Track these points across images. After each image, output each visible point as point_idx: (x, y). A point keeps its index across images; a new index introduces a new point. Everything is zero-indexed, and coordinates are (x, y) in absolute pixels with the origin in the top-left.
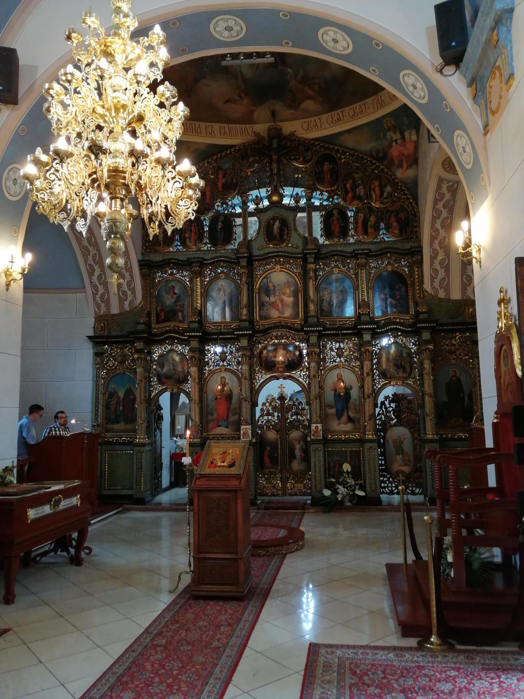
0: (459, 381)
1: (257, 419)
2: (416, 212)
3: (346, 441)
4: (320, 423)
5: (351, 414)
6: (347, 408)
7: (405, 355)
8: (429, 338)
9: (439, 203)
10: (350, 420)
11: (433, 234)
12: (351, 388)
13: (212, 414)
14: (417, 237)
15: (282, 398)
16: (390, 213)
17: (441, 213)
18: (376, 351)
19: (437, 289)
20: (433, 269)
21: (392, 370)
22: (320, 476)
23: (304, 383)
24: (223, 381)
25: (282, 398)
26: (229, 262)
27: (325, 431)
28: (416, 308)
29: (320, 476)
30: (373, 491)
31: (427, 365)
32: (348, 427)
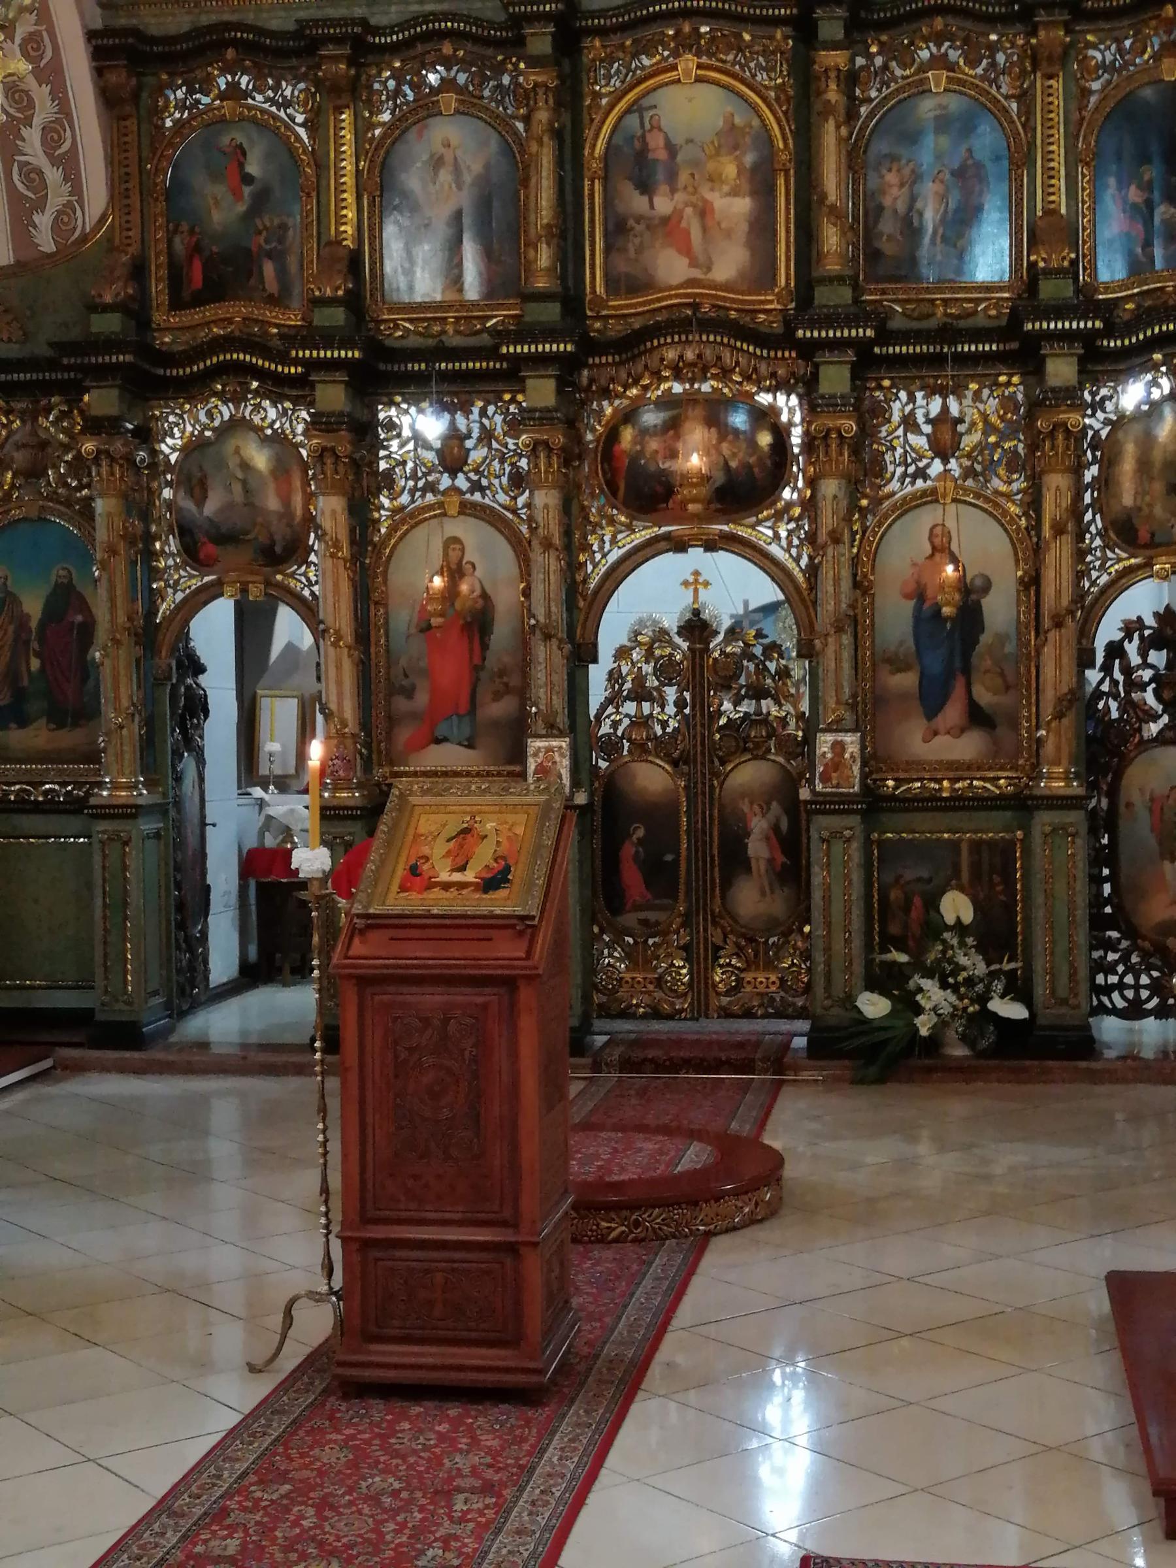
1: (593, 712)
3: (958, 803)
5: (984, 696)
6: (967, 671)
10: (978, 717)
12: (987, 587)
13: (409, 693)
18: (1097, 433)
22: (847, 942)
23: (791, 565)
26: (475, 39)
27: (871, 761)
29: (847, 942)
30: (1064, 1002)
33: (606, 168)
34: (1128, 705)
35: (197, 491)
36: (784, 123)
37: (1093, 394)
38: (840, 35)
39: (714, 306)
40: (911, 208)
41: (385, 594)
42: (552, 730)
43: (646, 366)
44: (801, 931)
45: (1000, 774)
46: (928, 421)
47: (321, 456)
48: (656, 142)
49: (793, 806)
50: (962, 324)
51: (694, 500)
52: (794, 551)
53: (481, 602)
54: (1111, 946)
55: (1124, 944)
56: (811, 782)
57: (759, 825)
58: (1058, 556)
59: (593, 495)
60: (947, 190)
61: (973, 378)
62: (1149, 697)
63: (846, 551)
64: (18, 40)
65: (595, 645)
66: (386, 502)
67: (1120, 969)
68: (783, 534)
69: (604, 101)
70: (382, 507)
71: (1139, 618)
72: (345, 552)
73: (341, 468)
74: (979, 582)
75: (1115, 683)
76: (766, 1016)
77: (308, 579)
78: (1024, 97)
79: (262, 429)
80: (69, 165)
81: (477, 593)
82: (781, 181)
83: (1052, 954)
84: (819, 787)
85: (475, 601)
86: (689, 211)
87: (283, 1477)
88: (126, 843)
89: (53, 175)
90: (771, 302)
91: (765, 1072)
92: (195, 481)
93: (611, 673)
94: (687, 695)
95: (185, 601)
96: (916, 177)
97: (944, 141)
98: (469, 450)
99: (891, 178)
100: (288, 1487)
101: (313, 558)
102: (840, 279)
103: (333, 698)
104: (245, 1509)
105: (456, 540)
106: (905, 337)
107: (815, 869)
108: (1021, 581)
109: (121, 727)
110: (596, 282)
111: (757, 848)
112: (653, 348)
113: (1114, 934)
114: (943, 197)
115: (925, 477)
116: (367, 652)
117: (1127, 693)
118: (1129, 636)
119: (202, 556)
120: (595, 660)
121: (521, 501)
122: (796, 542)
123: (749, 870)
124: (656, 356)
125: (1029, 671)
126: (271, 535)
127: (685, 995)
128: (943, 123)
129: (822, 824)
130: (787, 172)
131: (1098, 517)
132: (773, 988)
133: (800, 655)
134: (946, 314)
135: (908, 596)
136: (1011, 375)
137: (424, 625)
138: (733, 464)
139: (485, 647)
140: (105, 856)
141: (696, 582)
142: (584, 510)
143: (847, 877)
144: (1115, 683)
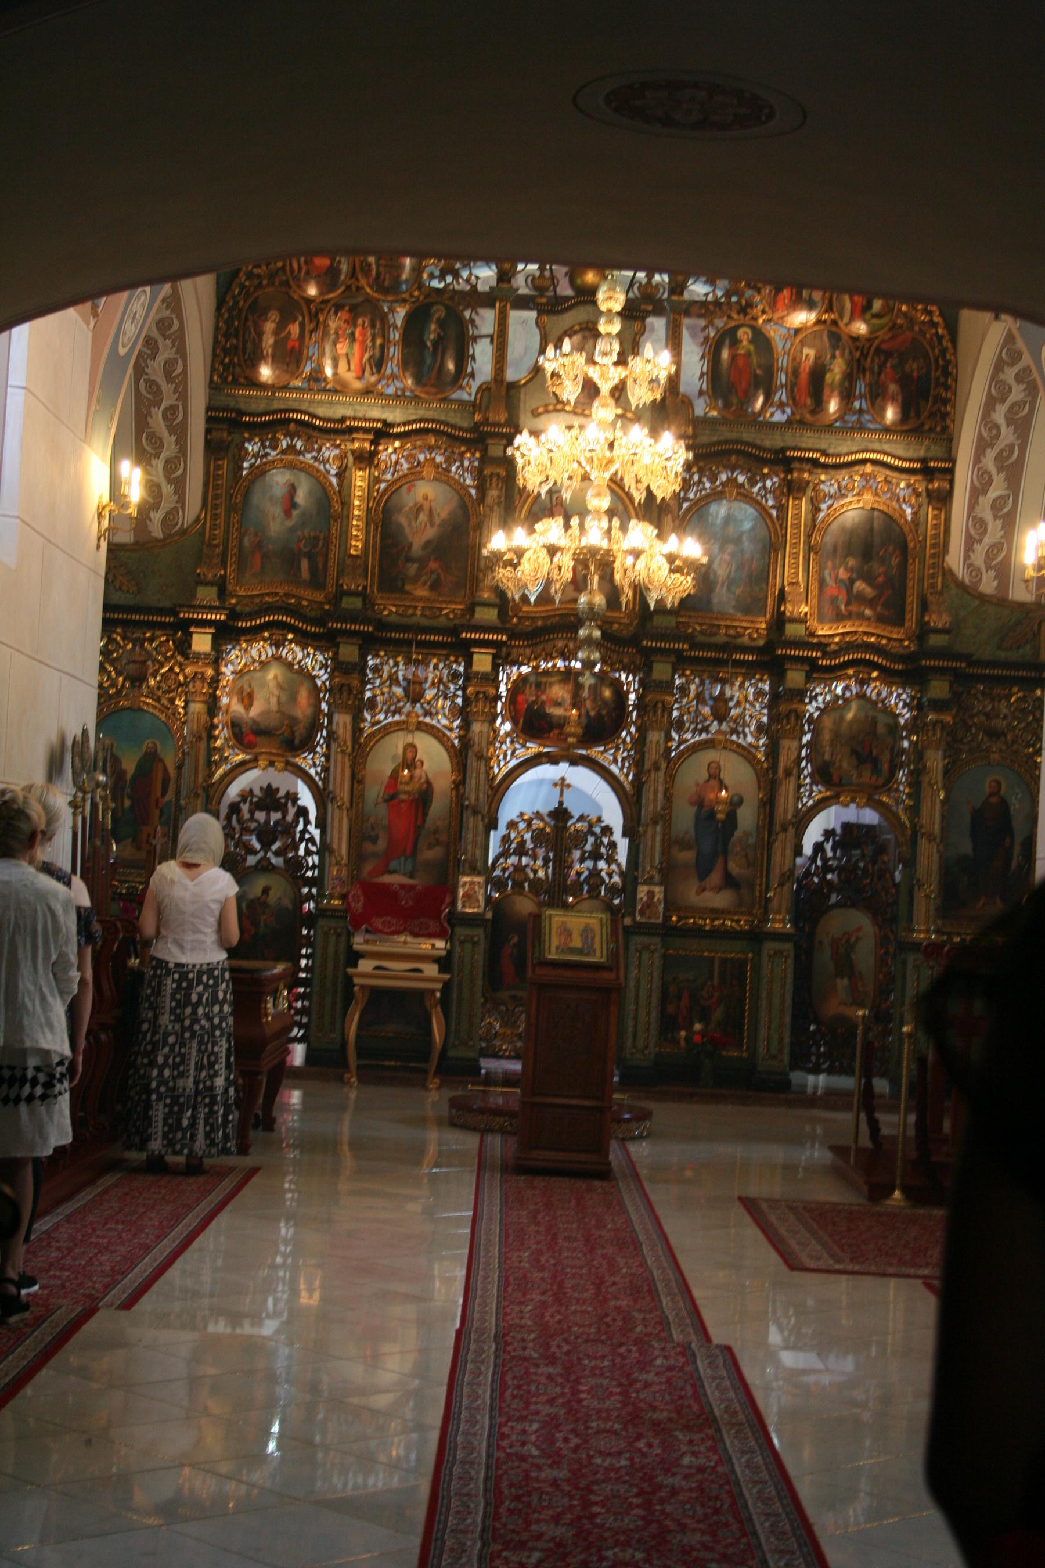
0: (1004, 807)
1: (490, 861)
2: (948, 362)
3: (717, 934)
4: (660, 884)
5: (734, 868)
6: (725, 853)
7: (881, 729)
8: (948, 696)
9: (1006, 369)
10: (730, 882)
11: (985, 434)
12: (740, 802)
13: (374, 840)
14: (945, 429)
15: (560, 814)
16: (882, 358)
17: (1010, 390)
18: (811, 715)
19: (979, 569)
20: (974, 518)
21: (845, 764)
22: (648, 1014)
23: (622, 778)
24: (410, 755)
25: (560, 814)
26: (449, 436)
27: (670, 904)
28: (923, 616)
29: (648, 1014)
30: (774, 1057)
31: (935, 761)
32: (721, 900)
35: (246, 700)
41: (363, 777)
43: (544, 649)
52: (625, 770)
61: (434, 655)
64: (162, 408)
68: (620, 760)
72: (349, 750)
78: (782, 508)
81: (423, 779)
92: (245, 694)
94: (551, 855)
98: (730, 709)
103: (336, 840)
108: (454, 782)
112: (549, 640)
115: (708, 732)
118: (827, 840)
119: (246, 741)
125: (762, 854)
126: (293, 733)
129: (638, 940)
131: (809, 766)
134: (726, 634)
135: (692, 804)
139: (425, 814)
143: (651, 974)
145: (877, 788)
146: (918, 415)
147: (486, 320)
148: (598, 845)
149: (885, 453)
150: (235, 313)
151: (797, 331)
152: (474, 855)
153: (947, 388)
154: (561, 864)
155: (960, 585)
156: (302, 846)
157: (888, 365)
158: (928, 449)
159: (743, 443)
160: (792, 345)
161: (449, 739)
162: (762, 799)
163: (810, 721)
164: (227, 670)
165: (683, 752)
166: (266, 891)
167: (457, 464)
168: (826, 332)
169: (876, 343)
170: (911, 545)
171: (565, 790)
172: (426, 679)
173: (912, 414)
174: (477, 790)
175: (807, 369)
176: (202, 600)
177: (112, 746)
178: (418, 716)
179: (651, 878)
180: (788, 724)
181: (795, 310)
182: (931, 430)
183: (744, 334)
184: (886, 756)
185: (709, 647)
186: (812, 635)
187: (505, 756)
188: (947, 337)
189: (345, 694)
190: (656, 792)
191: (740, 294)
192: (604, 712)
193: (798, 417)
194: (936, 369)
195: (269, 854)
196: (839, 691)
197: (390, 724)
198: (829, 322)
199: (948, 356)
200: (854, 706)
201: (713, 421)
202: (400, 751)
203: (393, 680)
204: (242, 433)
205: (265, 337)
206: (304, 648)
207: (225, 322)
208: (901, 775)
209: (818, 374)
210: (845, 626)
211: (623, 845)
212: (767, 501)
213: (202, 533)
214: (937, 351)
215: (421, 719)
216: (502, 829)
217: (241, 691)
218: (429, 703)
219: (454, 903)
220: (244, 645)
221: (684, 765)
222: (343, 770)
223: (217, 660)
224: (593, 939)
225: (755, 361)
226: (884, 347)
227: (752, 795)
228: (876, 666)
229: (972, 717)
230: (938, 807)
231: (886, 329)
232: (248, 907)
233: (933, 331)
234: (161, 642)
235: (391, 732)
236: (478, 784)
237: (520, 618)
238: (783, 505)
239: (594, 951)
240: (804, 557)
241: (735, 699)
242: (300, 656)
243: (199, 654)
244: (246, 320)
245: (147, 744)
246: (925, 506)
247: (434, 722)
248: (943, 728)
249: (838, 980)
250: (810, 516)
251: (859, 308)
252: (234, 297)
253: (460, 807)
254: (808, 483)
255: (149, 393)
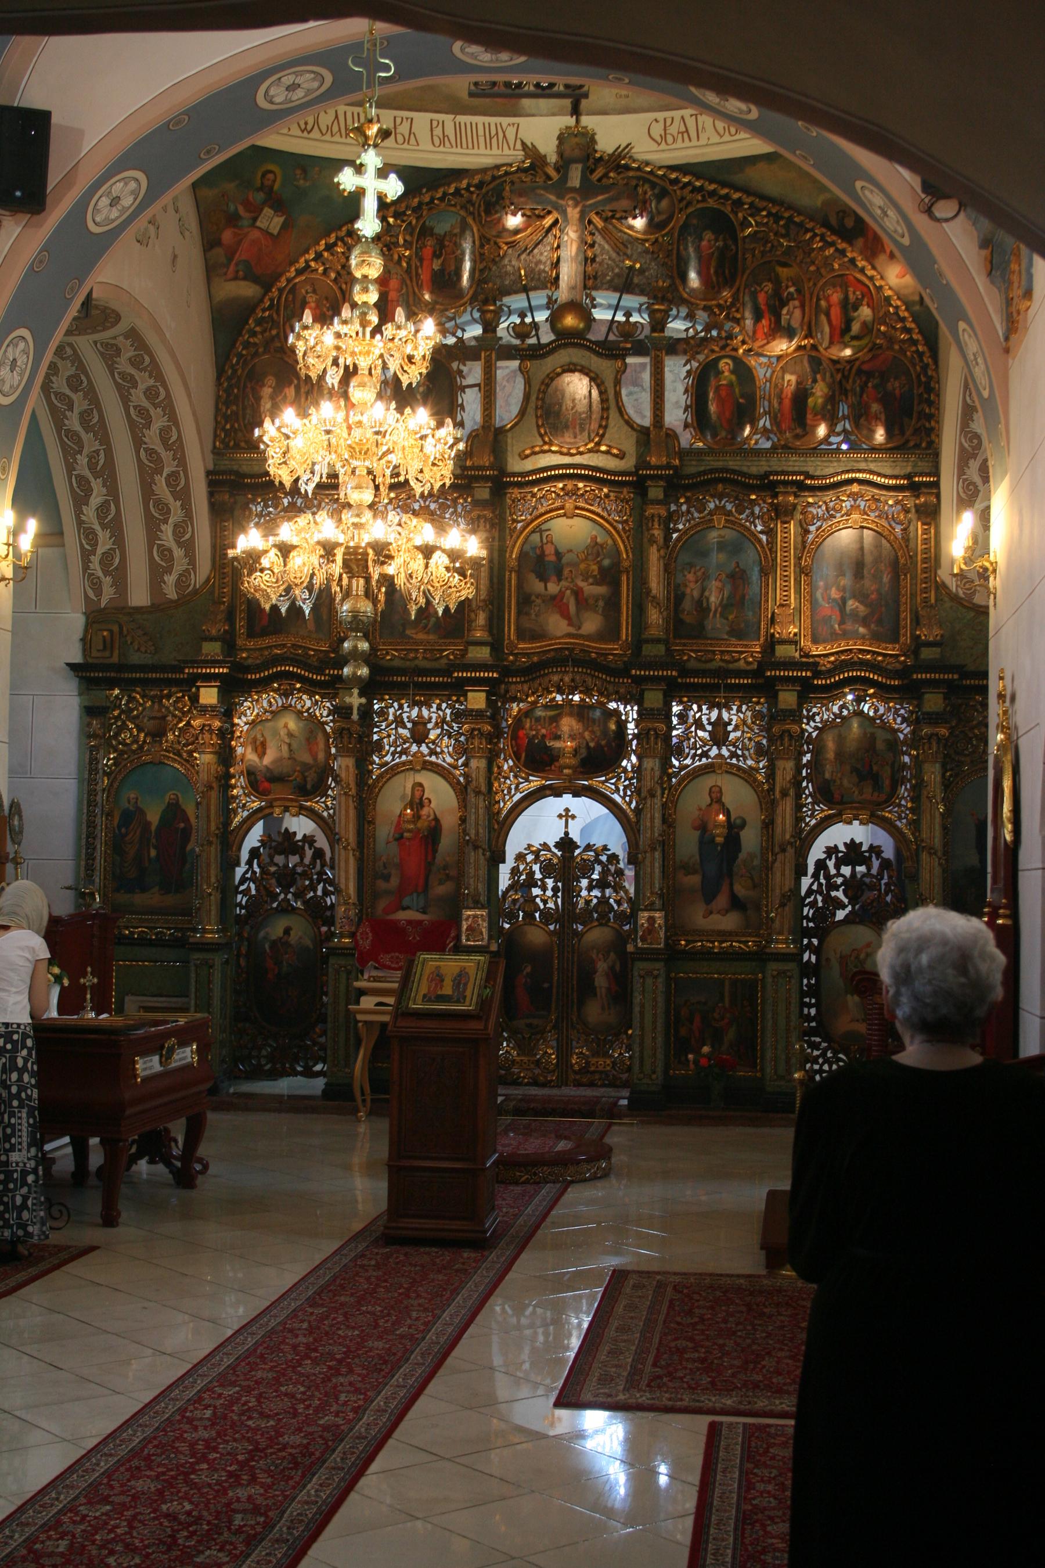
3: (726, 956)
5: (740, 890)
6: (730, 874)
7: (880, 745)
10: (736, 904)
11: (966, 445)
12: (743, 824)
13: (387, 878)
14: (931, 443)
15: (566, 844)
16: (864, 379)
22: (654, 1039)
24: (418, 794)
27: (674, 928)
29: (654, 1039)
32: (729, 922)
33: (519, 566)
34: (827, 899)
35: (260, 749)
36: (627, 543)
37: (808, 711)
38: (661, 496)
39: (581, 650)
40: (702, 595)
42: (477, 905)
44: (626, 1033)
45: (749, 939)
46: (710, 723)
47: (341, 733)
48: (549, 550)
49: (623, 955)
50: (731, 666)
51: (568, 767)
52: (627, 799)
53: (433, 823)
54: (815, 1046)
55: (824, 1045)
56: (635, 940)
57: (602, 966)
58: (787, 807)
59: (505, 760)
60: (724, 586)
61: (437, 696)
62: (839, 894)
63: (658, 802)
64: (164, 475)
65: (504, 852)
66: (377, 760)
67: (821, 1060)
68: (621, 788)
69: (519, 525)
70: (374, 762)
71: (836, 846)
72: (353, 792)
73: (353, 740)
74: (738, 822)
75: (820, 885)
76: (603, 1086)
77: (327, 806)
78: (770, 532)
79: (302, 713)
80: (189, 547)
81: (432, 817)
82: (624, 578)
83: (776, 1049)
84: (640, 944)
85: (430, 821)
86: (568, 592)
87: (106, 1500)
88: (211, 967)
89: (178, 553)
90: (616, 649)
91: (602, 1118)
92: (258, 743)
93: (513, 869)
94: (560, 884)
95: (248, 817)
96: (706, 577)
97: (722, 557)
99: (691, 577)
100: (108, 1507)
101: (330, 792)
102: (658, 641)
103: (343, 881)
104: (74, 1522)
105: (421, 785)
106: (696, 673)
107: (636, 994)
109: (210, 894)
110: (511, 631)
111: (601, 981)
113: (818, 1039)
114: (721, 590)
115: (708, 757)
116: (362, 853)
117: (828, 891)
119: (261, 789)
120: (504, 862)
121: (460, 762)
122: (629, 793)
123: (595, 995)
124: (546, 679)
127: (554, 1071)
128: (722, 546)
129: (641, 966)
130: (628, 572)
132: (608, 1068)
133: (630, 862)
134: (721, 660)
135: (696, 829)
136: (760, 698)
137: (397, 836)
138: (592, 745)
139: (435, 851)
140: (197, 975)
141: (567, 815)
142: (500, 768)
143: (655, 999)
144: (820, 885)
145: (879, 804)
146: (902, 433)
147: (473, 372)
148: (604, 873)
149: (871, 472)
150: (233, 381)
151: (779, 358)
152: (476, 889)
153: (930, 403)
154: (569, 892)
155: (955, 598)
156: (320, 887)
157: (870, 385)
158: (914, 466)
159: (727, 471)
160: (773, 372)
161: (454, 777)
162: (764, 820)
163: (809, 740)
164: (241, 722)
165: (683, 778)
166: (287, 931)
167: (451, 510)
168: (806, 357)
169: (857, 363)
170: (902, 561)
171: (570, 820)
172: (430, 718)
173: (897, 432)
174: (477, 824)
175: (789, 395)
176: (207, 655)
177: (137, 799)
178: (424, 756)
179: (653, 903)
180: (930, 749)
181: (774, 339)
182: (917, 446)
183: (725, 365)
184: (887, 772)
185: (704, 673)
186: (807, 655)
187: (509, 789)
188: (928, 354)
189: (345, 740)
190: (652, 819)
191: (719, 327)
192: (603, 743)
193: (783, 443)
194: (919, 386)
195: (290, 896)
196: (835, 709)
197: (397, 764)
198: (808, 347)
199: (930, 373)
200: (855, 724)
201: (699, 452)
202: (409, 791)
203: (399, 722)
204: (245, 495)
205: (262, 402)
206: (311, 695)
207: (225, 391)
208: (902, 791)
209: (801, 396)
210: (839, 646)
211: (630, 873)
212: (755, 526)
213: (212, 593)
214: (918, 368)
215: (428, 758)
216: (510, 862)
217: (255, 740)
218: (433, 742)
219: (458, 938)
220: (256, 697)
221: (685, 791)
222: (347, 811)
223: (228, 713)
224: (466, 985)
225: (737, 390)
226: (865, 367)
227: (754, 817)
228: (873, 683)
229: (972, 729)
230: (938, 820)
231: (865, 350)
232: (271, 947)
233: (913, 349)
234: (178, 698)
235: (398, 773)
236: (477, 819)
237: (515, 655)
238: (772, 530)
239: (465, 997)
240: (795, 580)
241: (734, 723)
242: (308, 703)
243: (206, 706)
244: (245, 386)
245: (169, 796)
246: (915, 522)
247: (440, 761)
248: (939, 740)
249: (849, 997)
250: (800, 538)
251: (838, 331)
252: (232, 366)
253: (465, 844)
254: (795, 506)
255: (150, 462)
